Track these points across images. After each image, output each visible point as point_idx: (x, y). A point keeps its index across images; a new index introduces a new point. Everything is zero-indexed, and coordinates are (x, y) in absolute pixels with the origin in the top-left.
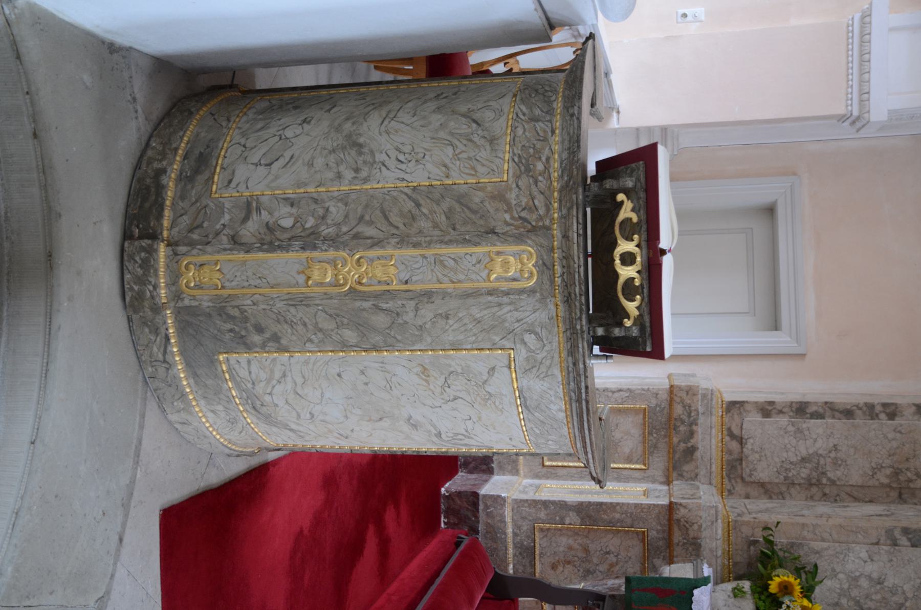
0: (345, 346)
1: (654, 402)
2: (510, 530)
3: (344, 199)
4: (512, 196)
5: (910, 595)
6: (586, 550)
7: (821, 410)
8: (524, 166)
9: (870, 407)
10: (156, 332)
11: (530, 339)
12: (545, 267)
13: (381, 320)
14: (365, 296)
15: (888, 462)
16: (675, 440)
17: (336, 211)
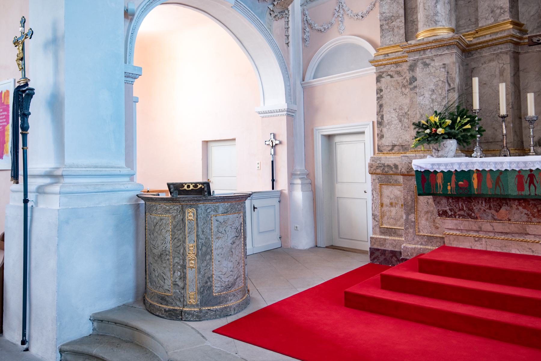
0: (211, 259)
1: (377, 181)
2: (419, 246)
3: (174, 258)
4: (174, 214)
5: (438, 79)
6: (427, 212)
7: (380, 116)
8: (168, 211)
9: (378, 98)
10: (207, 313)
11: (208, 211)
12: (191, 207)
13: (204, 249)
14: (198, 252)
15: (400, 90)
16: (391, 172)
17: (177, 260)
